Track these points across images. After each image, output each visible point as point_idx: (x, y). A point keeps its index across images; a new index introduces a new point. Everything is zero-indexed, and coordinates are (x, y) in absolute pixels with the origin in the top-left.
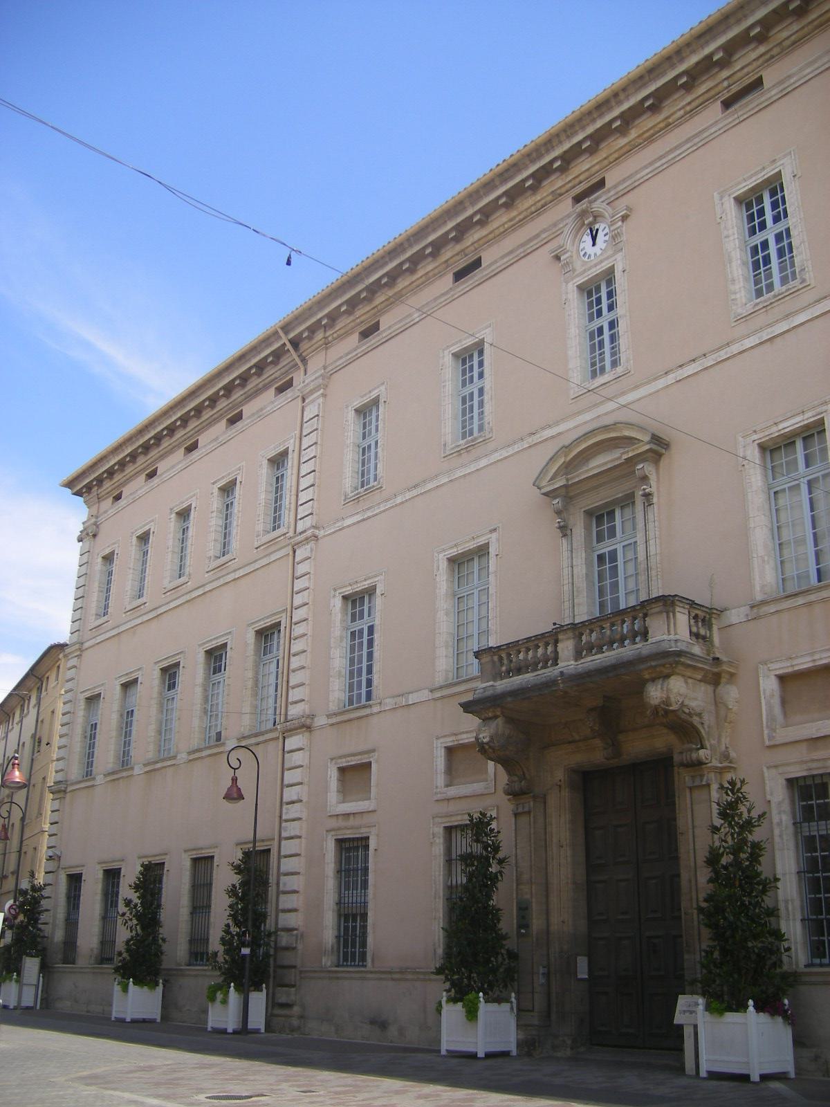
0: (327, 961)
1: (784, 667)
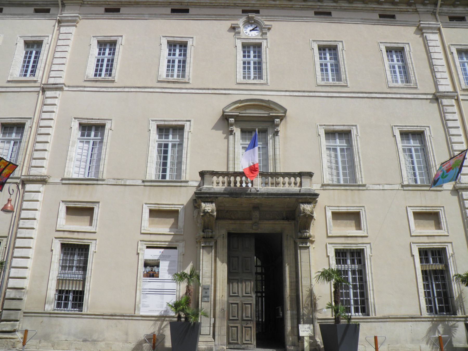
0: (50, 308)
1: (336, 210)
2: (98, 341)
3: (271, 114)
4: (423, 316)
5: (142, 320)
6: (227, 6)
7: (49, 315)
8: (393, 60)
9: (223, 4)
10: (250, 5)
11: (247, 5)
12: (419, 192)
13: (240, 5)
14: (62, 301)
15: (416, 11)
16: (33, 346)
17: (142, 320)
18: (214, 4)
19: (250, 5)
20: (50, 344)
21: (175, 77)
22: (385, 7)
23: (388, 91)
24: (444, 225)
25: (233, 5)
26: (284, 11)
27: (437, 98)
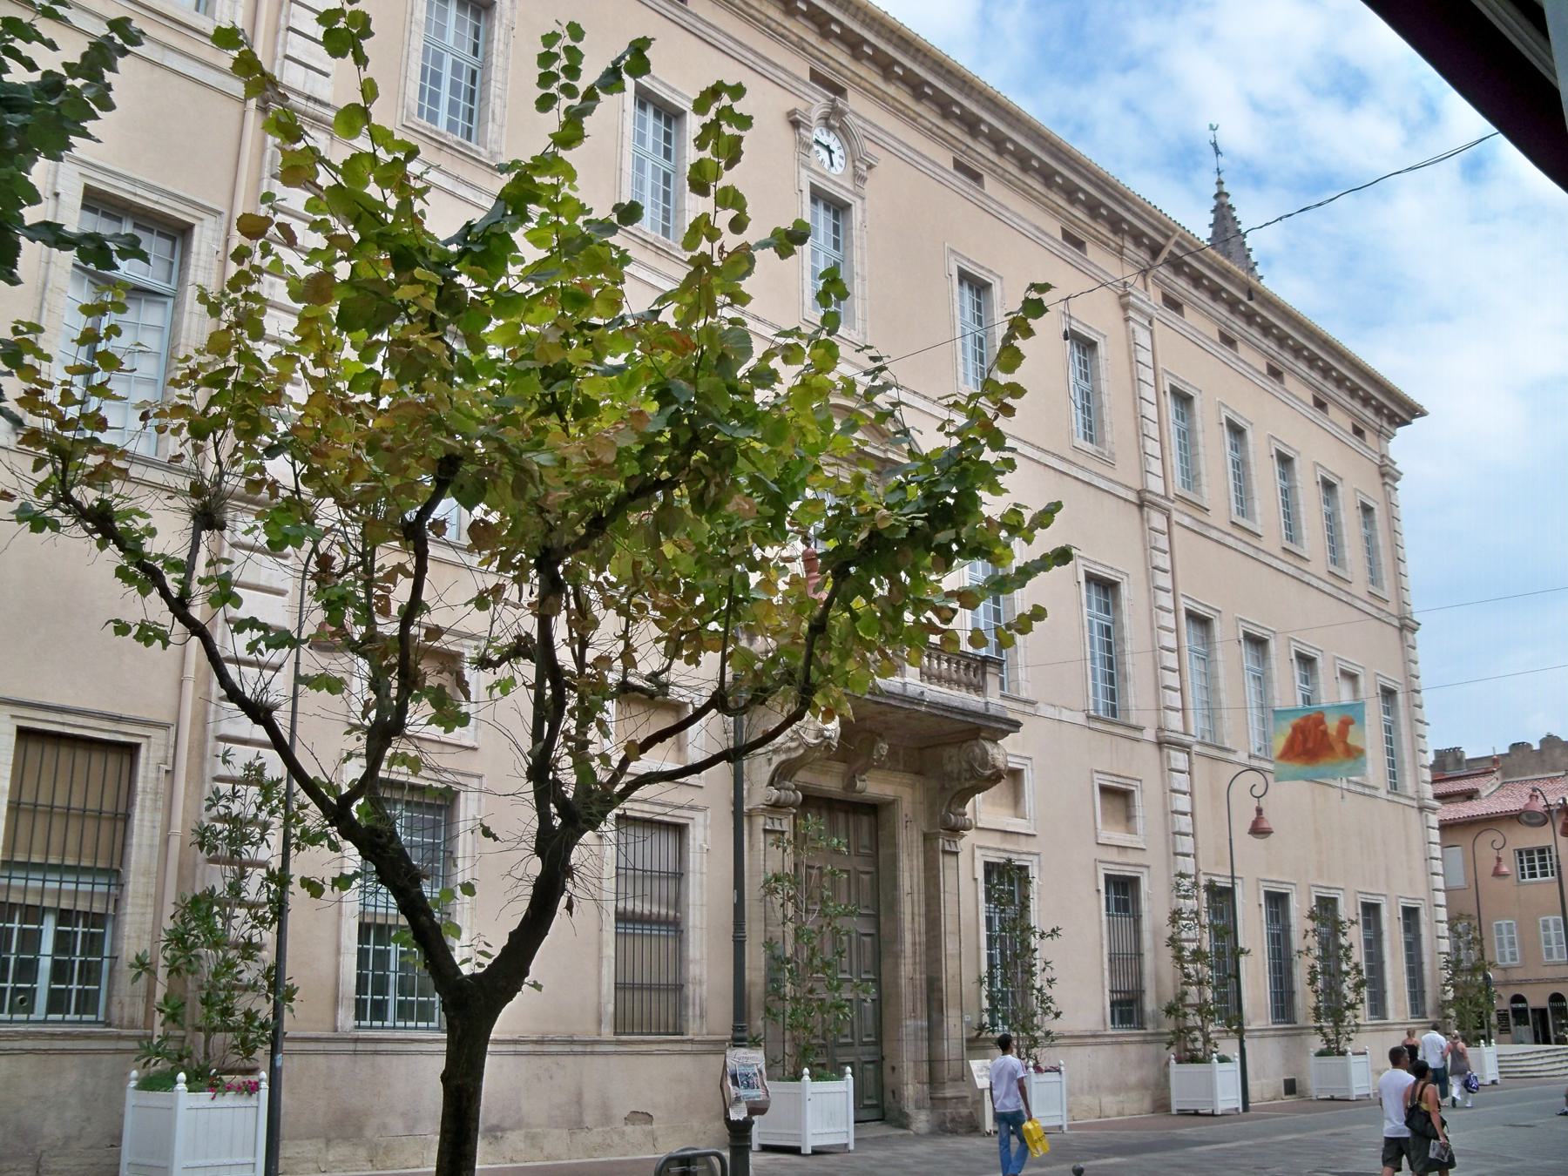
2: (503, 1130)
3: (890, 455)
4: (604, 1038)
5: (616, 1053)
6: (782, 36)
7: (351, 1047)
8: (441, 31)
9: (774, 25)
10: (831, 63)
11: (826, 59)
12: (1107, 738)
13: (810, 49)
14: (79, 991)
15: (1120, 252)
16: (307, 1161)
17: (616, 1053)
18: (752, 12)
19: (831, 63)
20: (362, 1153)
21: (442, 126)
22: (980, 149)
23: (1070, 456)
24: (1139, 823)
25: (795, 39)
26: (894, 120)
27: (1143, 502)
